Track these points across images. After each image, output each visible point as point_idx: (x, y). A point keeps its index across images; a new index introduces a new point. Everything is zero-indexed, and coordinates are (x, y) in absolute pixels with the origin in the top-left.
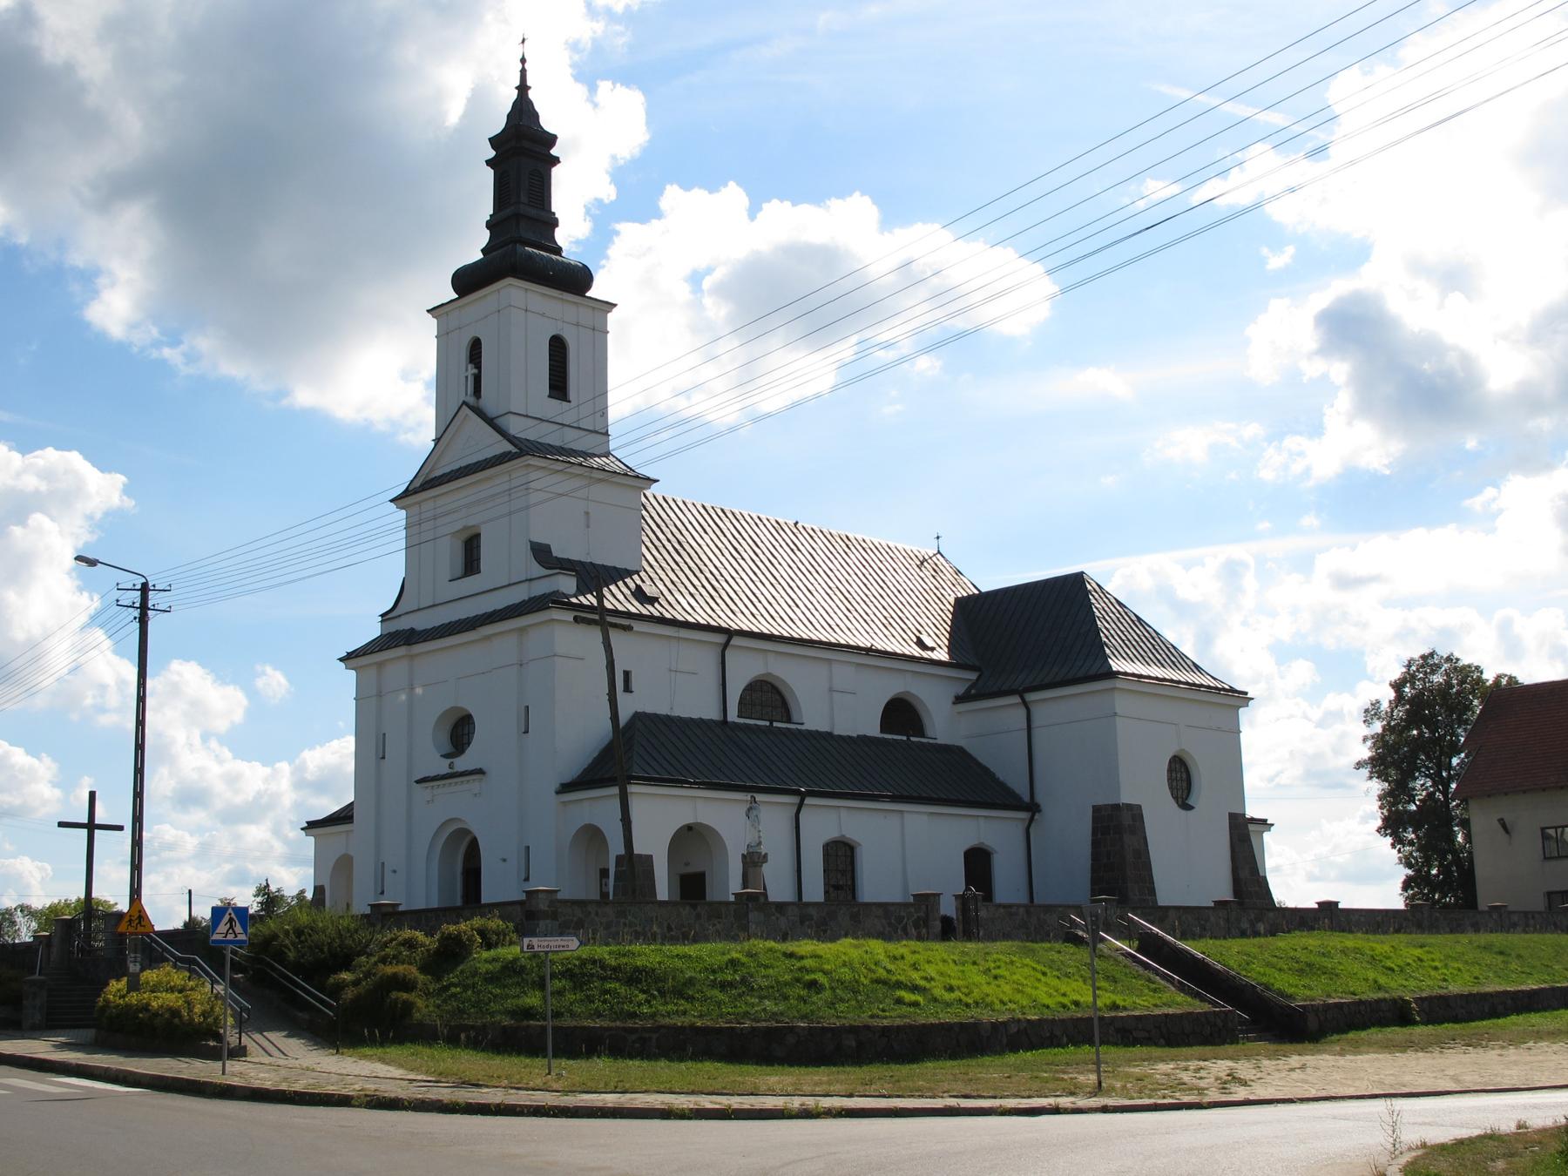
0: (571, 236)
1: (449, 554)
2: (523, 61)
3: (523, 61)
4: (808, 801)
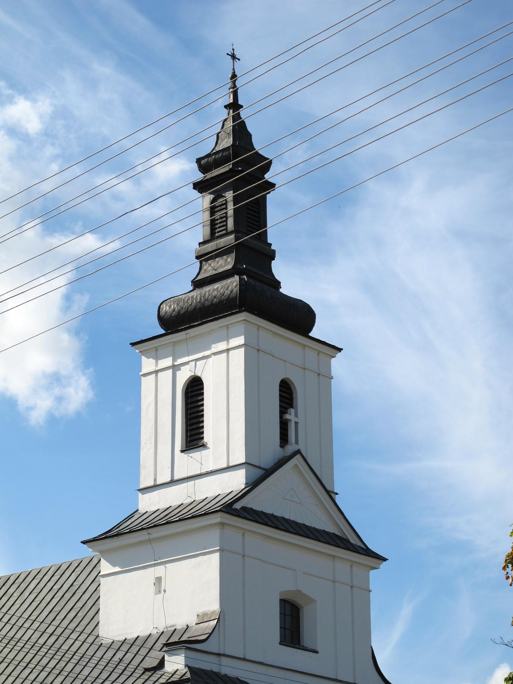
0: (292, 280)
1: (317, 625)
3: (234, 76)
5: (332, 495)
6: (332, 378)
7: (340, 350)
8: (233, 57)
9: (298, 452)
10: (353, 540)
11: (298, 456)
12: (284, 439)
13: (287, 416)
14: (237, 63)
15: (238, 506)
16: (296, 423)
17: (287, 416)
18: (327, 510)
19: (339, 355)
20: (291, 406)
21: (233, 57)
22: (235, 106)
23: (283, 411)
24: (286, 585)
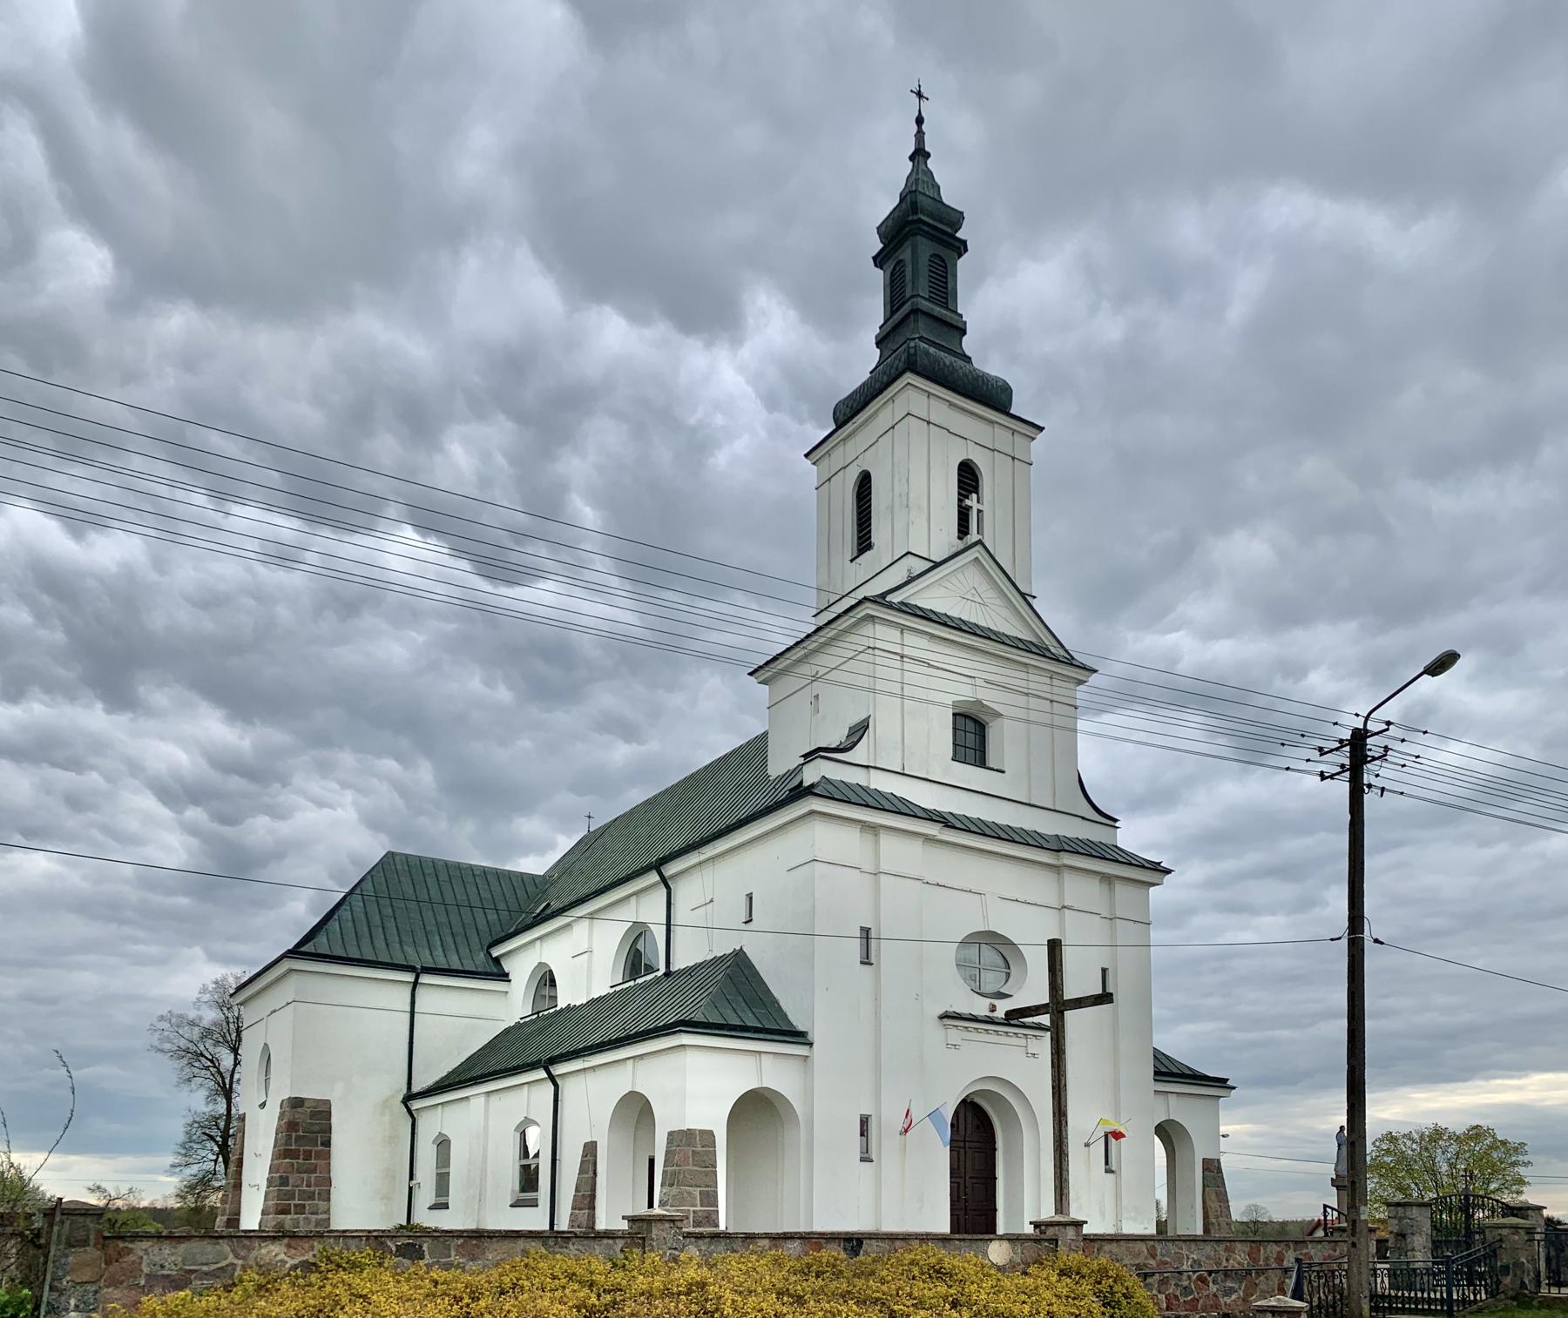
0: (984, 352)
2: (920, 121)
3: (920, 121)
4: (425, 979)
5: (549, 911)
6: (961, 248)
7: (1041, 429)
8: (919, 95)
9: (980, 542)
10: (1048, 641)
11: (979, 547)
12: (963, 529)
13: (968, 502)
14: (924, 103)
15: (895, 598)
16: (979, 511)
17: (968, 502)
18: (791, 822)
19: (1040, 436)
20: (976, 489)
21: (919, 95)
22: (920, 155)
23: (962, 496)
24: (964, 692)
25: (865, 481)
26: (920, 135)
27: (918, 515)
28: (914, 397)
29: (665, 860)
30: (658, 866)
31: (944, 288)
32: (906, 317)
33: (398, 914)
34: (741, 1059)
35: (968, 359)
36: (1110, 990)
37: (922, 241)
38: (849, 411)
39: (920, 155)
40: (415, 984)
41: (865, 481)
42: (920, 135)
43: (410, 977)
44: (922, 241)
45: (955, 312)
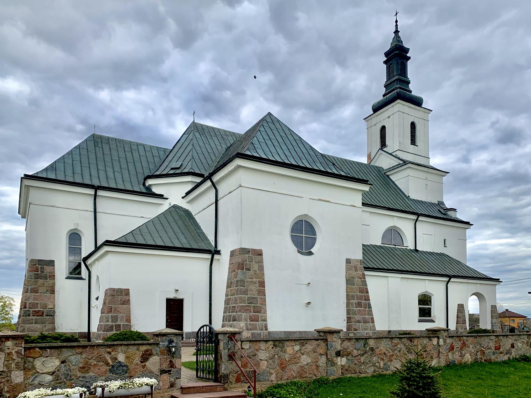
0: (415, 89)
2: (396, 22)
3: (396, 22)
22: (397, 32)
25: (383, 128)
26: (397, 25)
27: (397, 140)
28: (399, 106)
29: (422, 215)
30: (418, 215)
31: (403, 71)
32: (394, 81)
33: (91, 166)
34: (440, 283)
35: (411, 92)
36: (219, 249)
37: (397, 57)
38: (377, 109)
39: (397, 32)
40: (417, 220)
41: (383, 128)
42: (397, 25)
43: (415, 217)
44: (397, 57)
45: (407, 78)
